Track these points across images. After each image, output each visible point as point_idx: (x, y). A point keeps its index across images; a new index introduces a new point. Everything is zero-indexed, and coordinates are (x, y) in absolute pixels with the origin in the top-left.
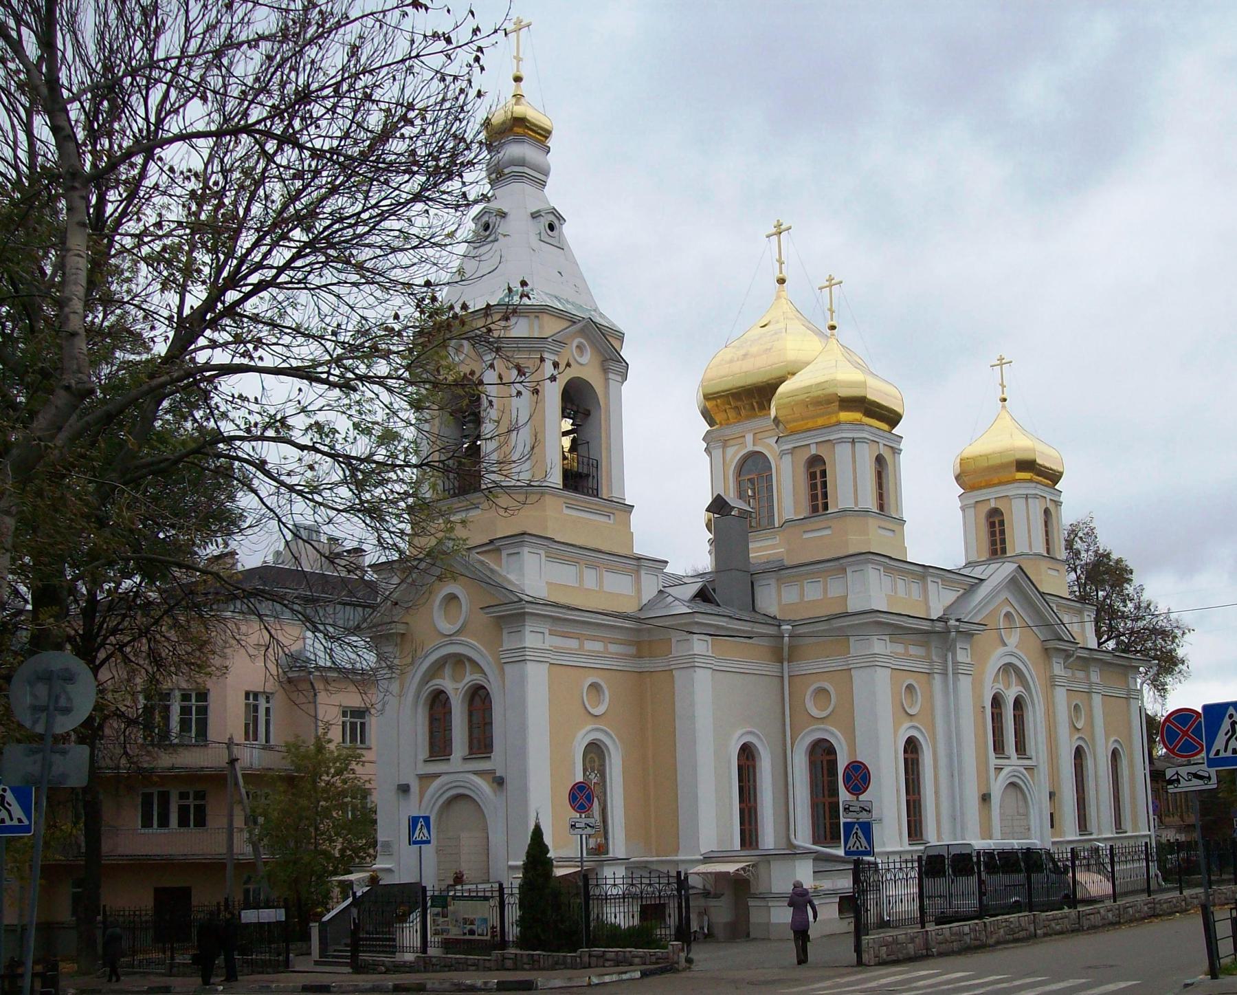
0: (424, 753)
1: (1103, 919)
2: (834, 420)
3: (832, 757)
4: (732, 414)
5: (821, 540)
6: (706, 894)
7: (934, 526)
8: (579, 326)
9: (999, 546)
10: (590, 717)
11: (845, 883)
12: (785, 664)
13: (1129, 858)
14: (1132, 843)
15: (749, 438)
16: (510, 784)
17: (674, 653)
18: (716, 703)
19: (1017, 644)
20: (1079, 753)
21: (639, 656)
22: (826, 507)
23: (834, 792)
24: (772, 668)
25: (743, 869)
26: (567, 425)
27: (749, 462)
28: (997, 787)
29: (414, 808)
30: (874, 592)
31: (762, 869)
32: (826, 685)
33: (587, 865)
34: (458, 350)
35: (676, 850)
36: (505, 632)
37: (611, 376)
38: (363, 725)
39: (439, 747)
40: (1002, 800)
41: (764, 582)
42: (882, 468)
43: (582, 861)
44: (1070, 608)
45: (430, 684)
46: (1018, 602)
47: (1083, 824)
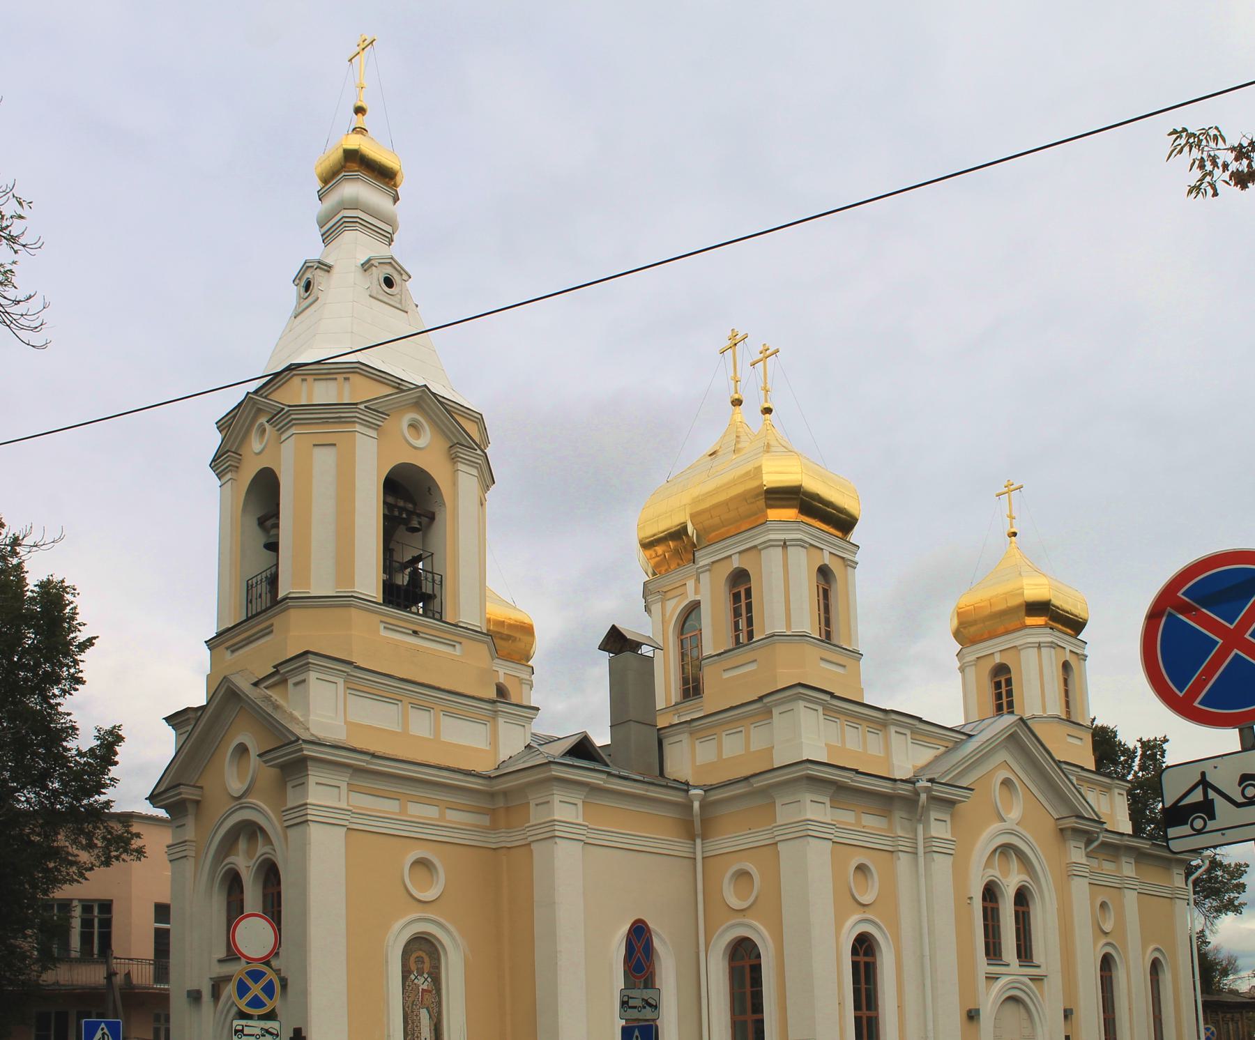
8: (416, 393)
10: (415, 903)
12: (699, 841)
19: (1017, 814)
20: (1107, 963)
21: (494, 827)
22: (750, 635)
24: (680, 847)
32: (749, 867)
36: (289, 785)
37: (461, 467)
46: (1042, 792)
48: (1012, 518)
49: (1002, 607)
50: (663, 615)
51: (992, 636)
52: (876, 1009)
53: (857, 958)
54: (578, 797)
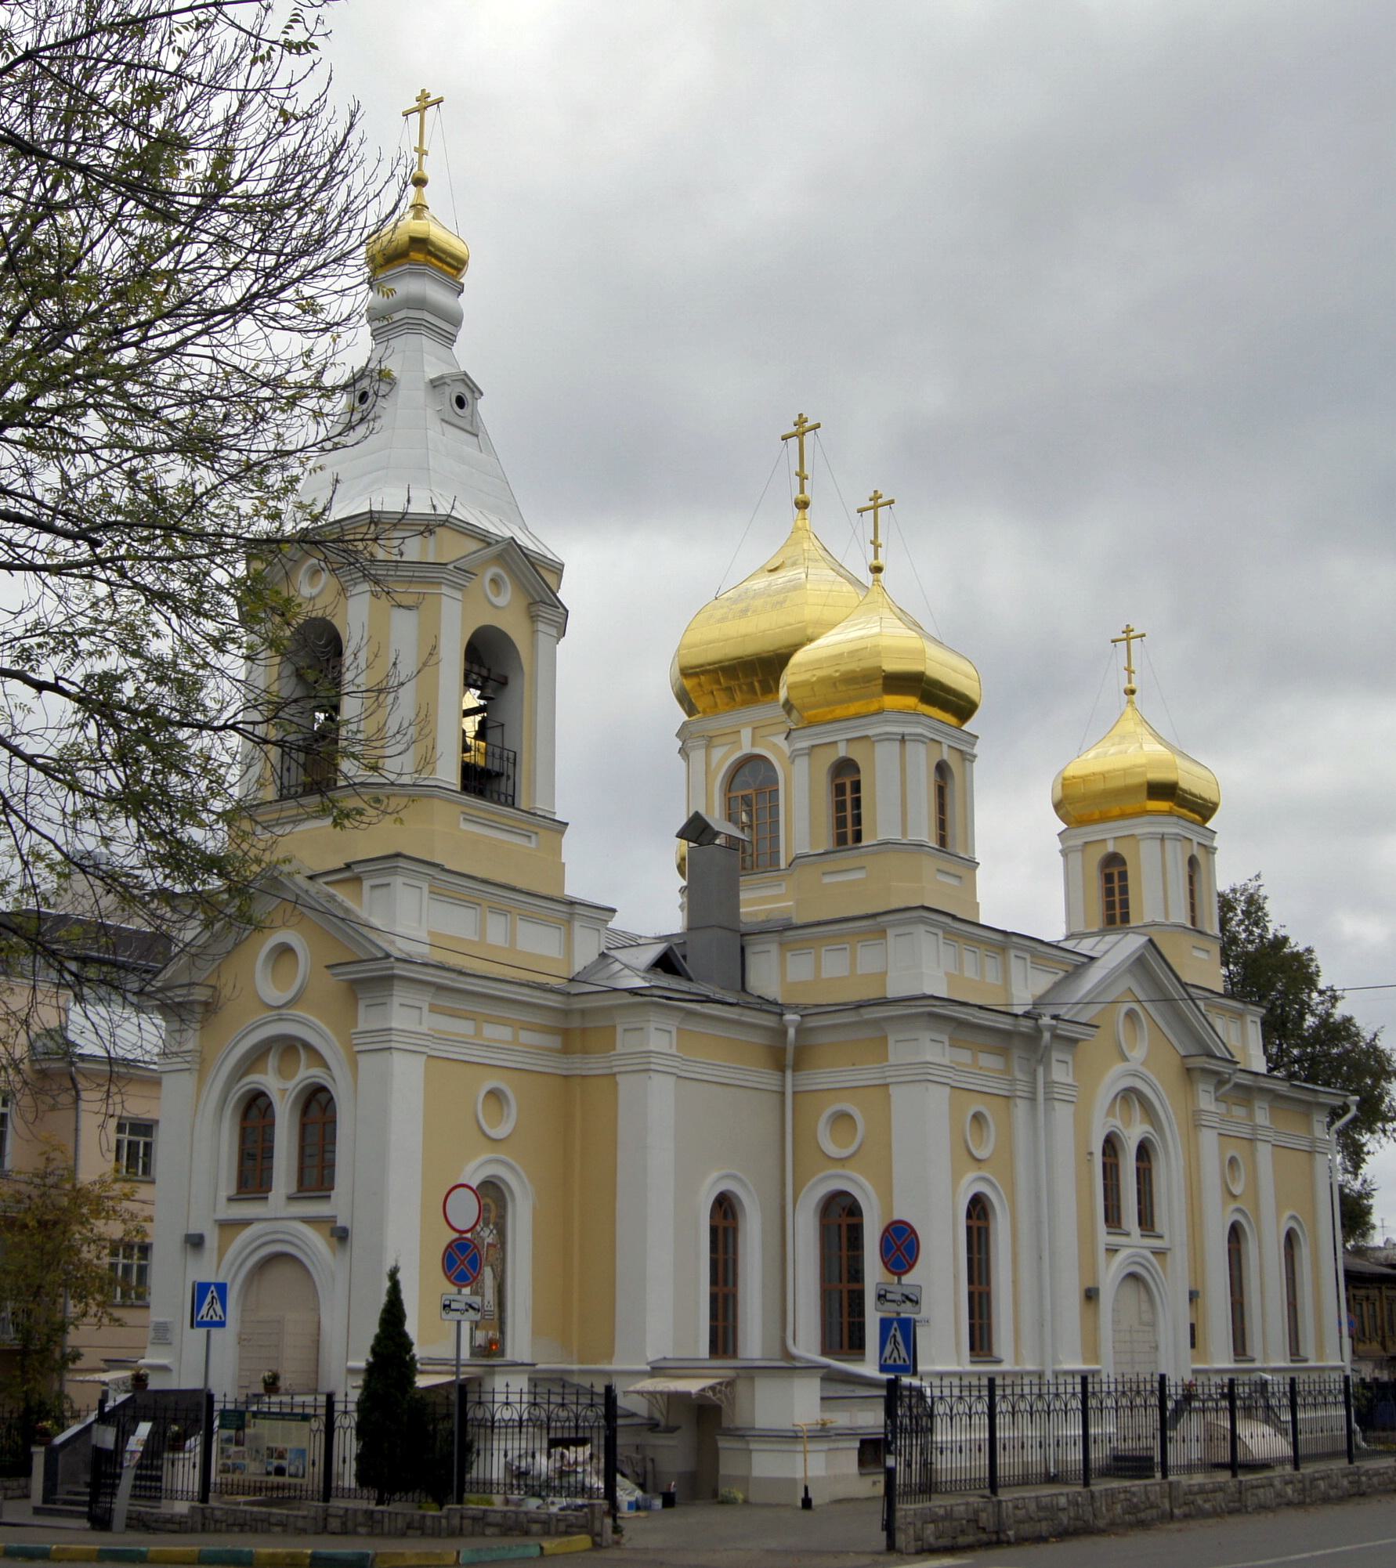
0: (227, 1183)
1: (1278, 1495)
2: (874, 707)
3: (852, 1220)
4: (721, 698)
5: (850, 886)
6: (653, 1426)
7: (1021, 874)
8: (499, 547)
9: (1118, 912)
11: (871, 1419)
12: (789, 1074)
13: (1320, 1399)
14: (1314, 1376)
15: (746, 734)
16: (357, 1238)
17: (619, 1049)
18: (679, 1126)
19: (1141, 1056)
20: (1235, 1233)
21: (566, 1050)
22: (858, 837)
23: (856, 1274)
24: (768, 1079)
25: (712, 1388)
26: (472, 699)
27: (746, 770)
29: (205, 1270)
30: (926, 968)
31: (741, 1387)
33: (466, 1373)
34: (315, 572)
35: (609, 1356)
36: (361, 1005)
37: (541, 626)
38: (148, 1146)
39: (253, 1176)
40: (1116, 1300)
42: (945, 781)
43: (458, 1365)
44: (1222, 1007)
47: (1240, 1346)
49: (1119, 783)
50: (708, 764)
51: (1104, 818)
52: (988, 1283)
53: (971, 1223)
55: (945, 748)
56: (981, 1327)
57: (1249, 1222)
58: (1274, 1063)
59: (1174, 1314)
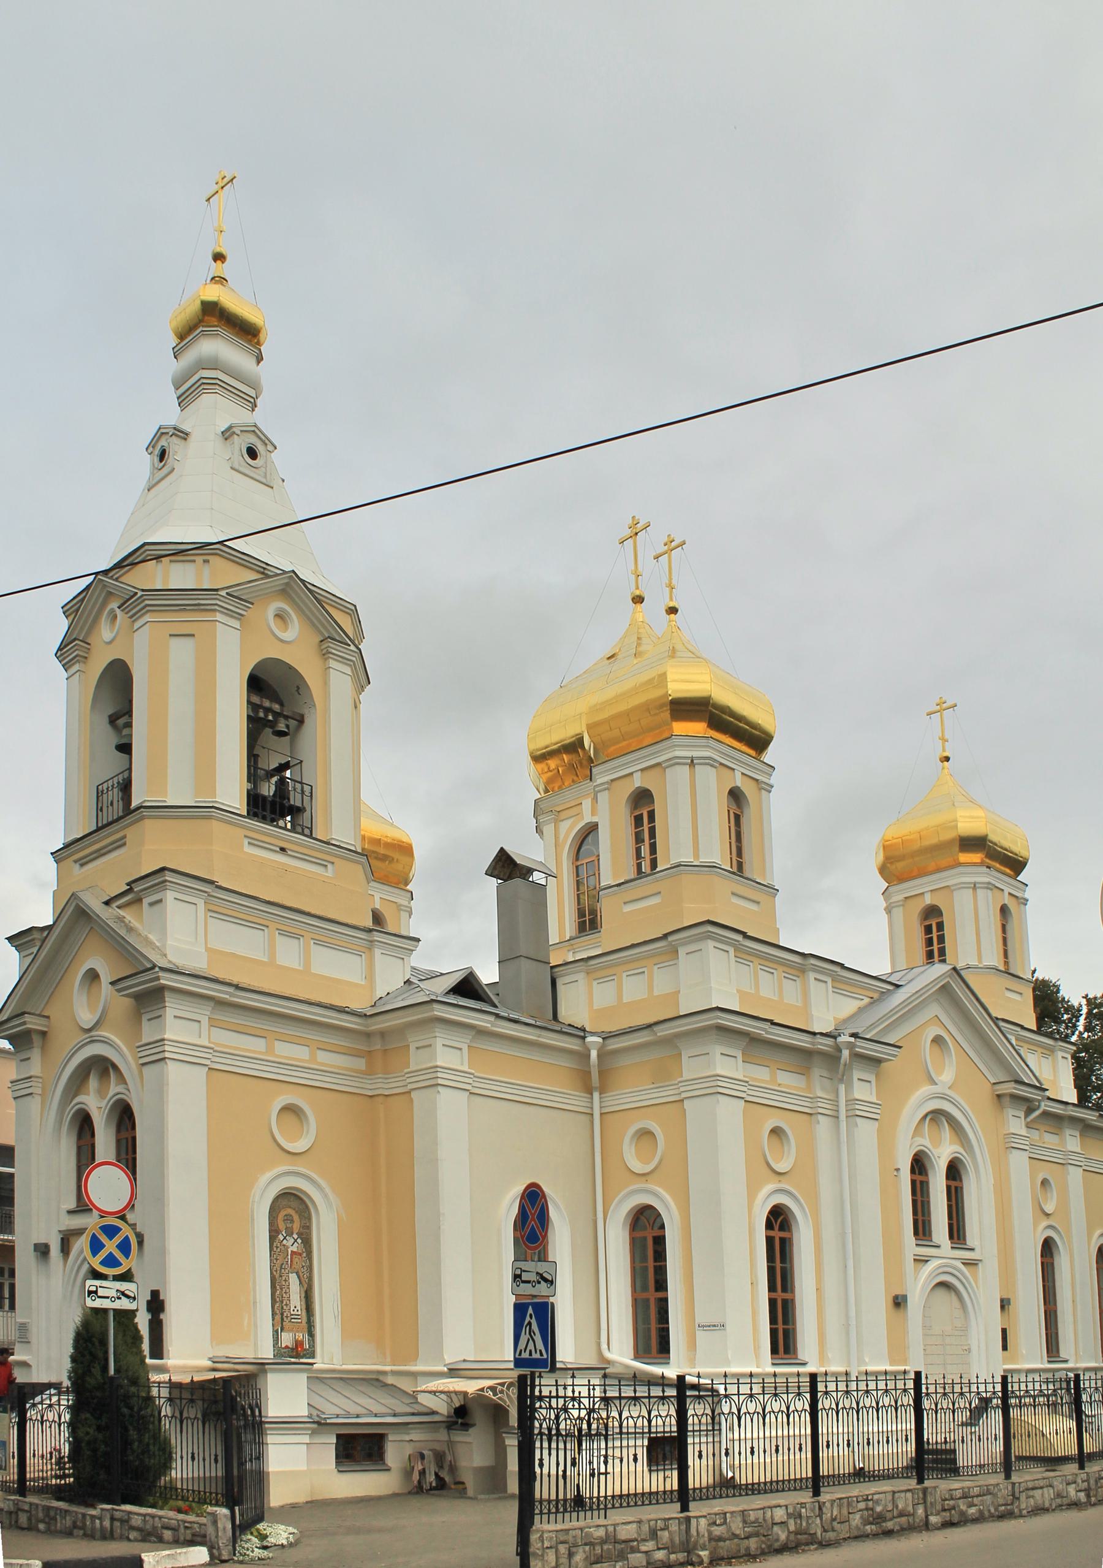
12: (596, 1095)
21: (370, 1072)
22: (654, 864)
24: (576, 1101)
28: (918, 1285)
36: (145, 1018)
37: (332, 663)
41: (567, 979)
45: (74, 1102)
46: (955, 1023)
48: (944, 740)
50: (556, 837)
51: (922, 873)
54: (463, 1041)
55: (738, 775)
56: (786, 1333)
57: (1064, 1243)
58: (1083, 1100)
59: (986, 1322)
